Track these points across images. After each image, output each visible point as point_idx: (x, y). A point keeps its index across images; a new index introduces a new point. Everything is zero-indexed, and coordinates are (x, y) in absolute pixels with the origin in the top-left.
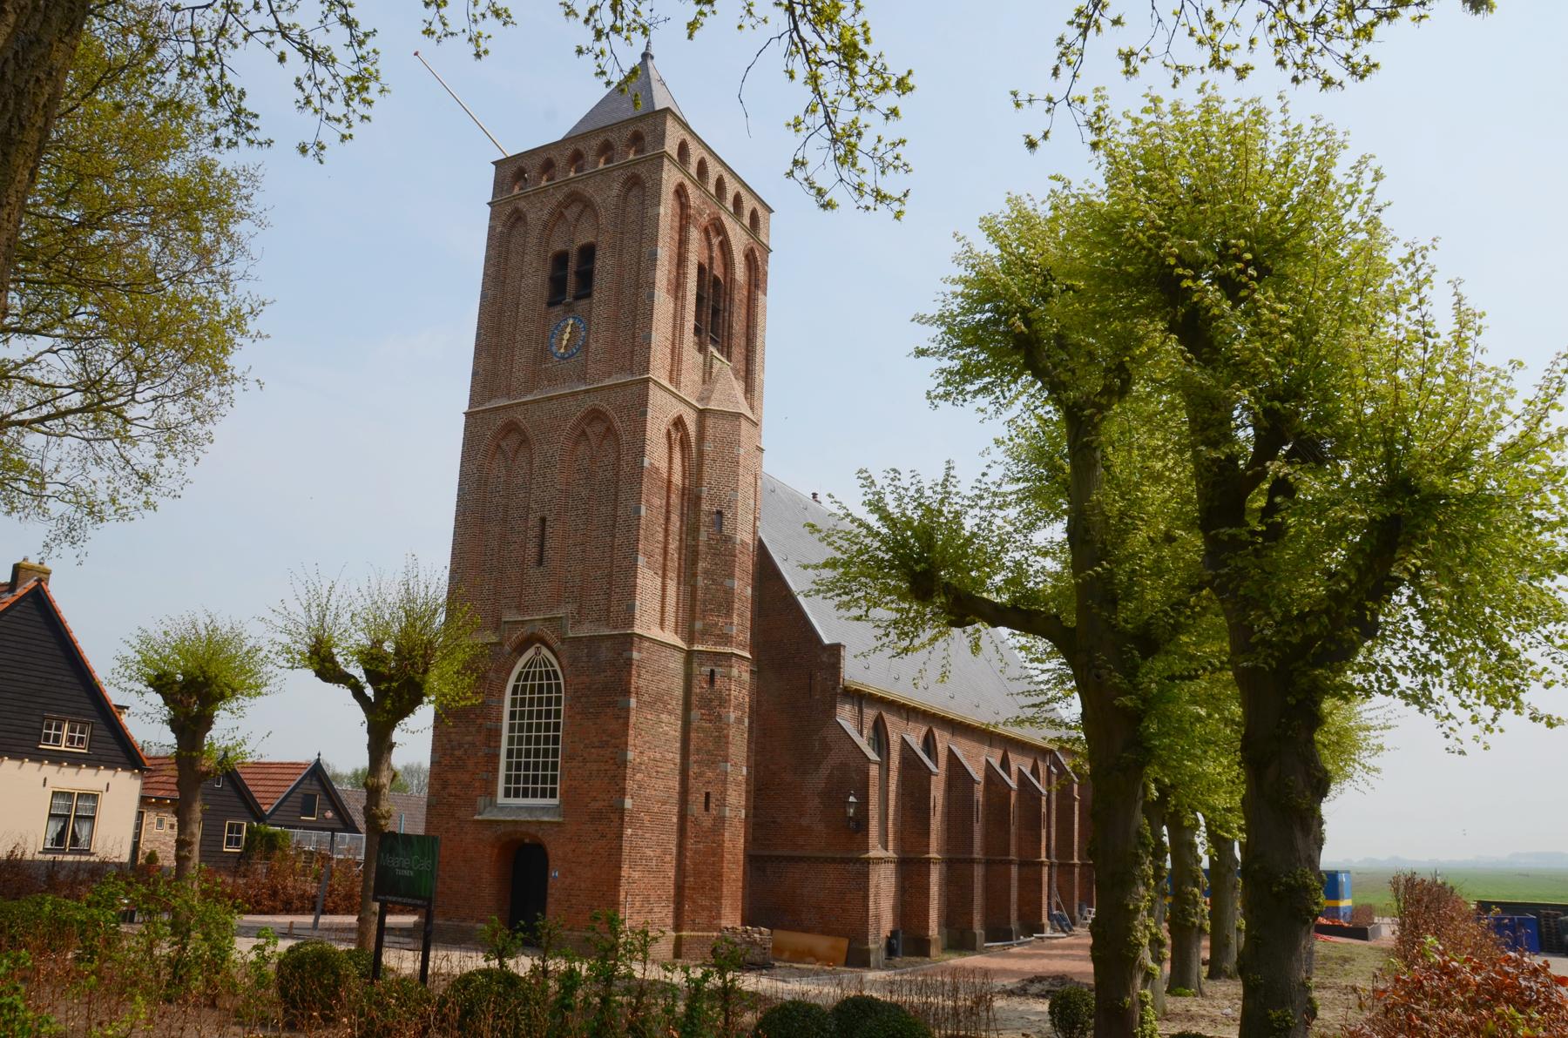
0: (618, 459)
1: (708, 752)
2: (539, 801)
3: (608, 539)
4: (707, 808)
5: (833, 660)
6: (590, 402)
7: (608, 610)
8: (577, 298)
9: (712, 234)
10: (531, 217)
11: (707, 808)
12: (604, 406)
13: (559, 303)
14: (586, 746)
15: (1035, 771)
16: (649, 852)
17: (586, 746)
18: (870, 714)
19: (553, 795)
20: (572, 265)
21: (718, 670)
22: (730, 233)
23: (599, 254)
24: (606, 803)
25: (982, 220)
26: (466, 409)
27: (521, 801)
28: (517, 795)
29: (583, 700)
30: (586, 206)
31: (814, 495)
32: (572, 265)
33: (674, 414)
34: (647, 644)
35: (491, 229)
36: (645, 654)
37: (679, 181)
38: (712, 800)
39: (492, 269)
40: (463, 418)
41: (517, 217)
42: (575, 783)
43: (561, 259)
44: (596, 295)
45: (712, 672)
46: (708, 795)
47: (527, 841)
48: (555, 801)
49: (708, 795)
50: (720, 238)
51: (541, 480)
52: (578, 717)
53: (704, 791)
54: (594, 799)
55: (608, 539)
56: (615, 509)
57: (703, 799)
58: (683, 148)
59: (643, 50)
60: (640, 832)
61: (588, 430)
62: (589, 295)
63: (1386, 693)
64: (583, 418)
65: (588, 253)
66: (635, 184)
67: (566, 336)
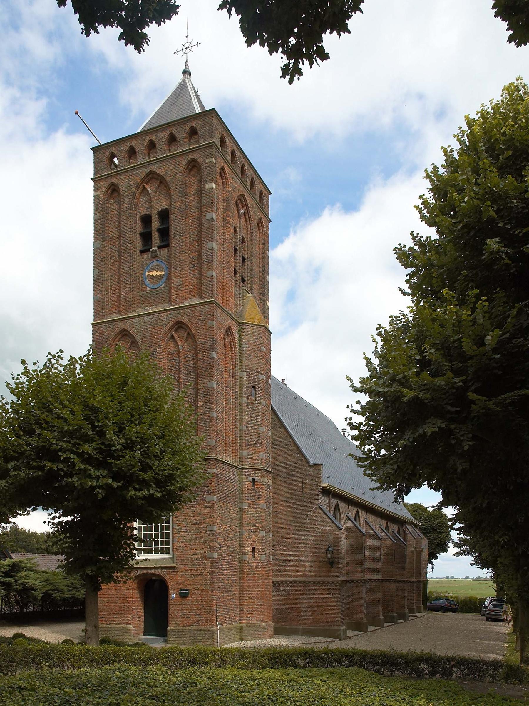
1: (253, 525)
4: (254, 556)
5: (316, 472)
6: (121, 326)
8: (160, 247)
9: (240, 206)
10: (123, 188)
11: (254, 556)
12: (128, 327)
13: (148, 250)
15: (399, 532)
18: (334, 501)
20: (156, 224)
23: (172, 217)
26: (92, 321)
30: (161, 182)
31: (283, 380)
32: (156, 224)
33: (226, 324)
35: (95, 197)
38: (257, 551)
39: (100, 226)
40: (91, 328)
41: (114, 189)
42: (182, 545)
43: (146, 220)
46: (254, 548)
47: (154, 578)
49: (254, 548)
53: (251, 547)
54: (195, 553)
57: (251, 551)
58: (223, 141)
59: (184, 68)
60: (221, 571)
61: (175, 334)
65: (164, 215)
66: (194, 166)
67: (155, 273)
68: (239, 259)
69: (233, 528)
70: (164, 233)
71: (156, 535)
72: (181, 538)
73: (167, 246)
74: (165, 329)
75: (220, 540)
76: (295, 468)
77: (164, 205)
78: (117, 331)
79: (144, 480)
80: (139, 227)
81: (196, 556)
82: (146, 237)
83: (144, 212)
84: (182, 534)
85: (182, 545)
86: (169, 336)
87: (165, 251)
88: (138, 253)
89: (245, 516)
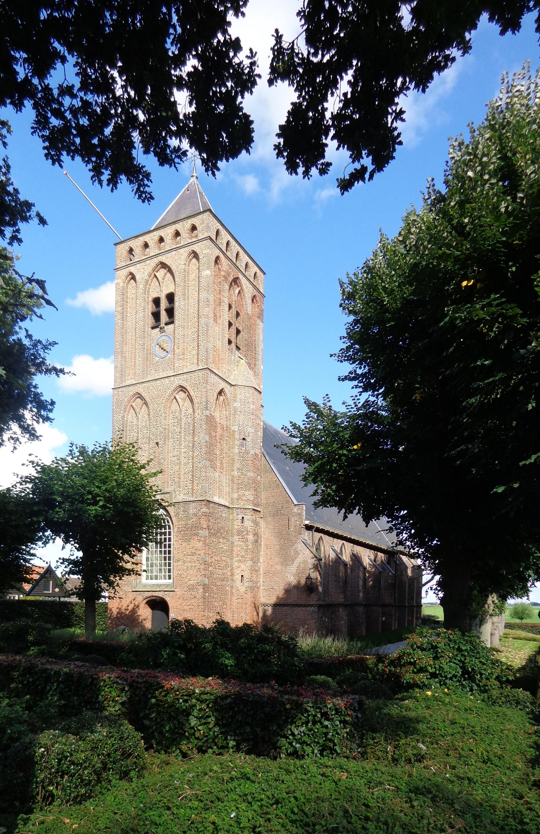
0: (194, 412)
2: (163, 581)
3: (191, 453)
7: (193, 489)
8: (167, 324)
12: (184, 384)
14: (185, 555)
16: (216, 604)
17: (185, 555)
19: (170, 578)
20: (164, 304)
21: (245, 517)
22: (244, 287)
24: (196, 582)
25: (298, 14)
27: (154, 582)
28: (152, 579)
29: (182, 533)
32: (164, 304)
34: (212, 505)
36: (211, 510)
37: (217, 255)
42: (180, 572)
43: (157, 301)
44: (176, 322)
45: (243, 518)
48: (171, 581)
50: (239, 288)
51: (155, 423)
52: (180, 541)
55: (191, 453)
56: (193, 438)
62: (172, 322)
63: (40, 342)
64: (174, 391)
65: (171, 297)
68: (233, 330)
69: (224, 558)
70: (170, 312)
71: (165, 539)
72: (179, 567)
73: (172, 322)
74: (169, 392)
75: (210, 569)
76: (282, 507)
77: (171, 290)
78: (131, 393)
79: (286, 694)
80: (150, 307)
81: (191, 582)
82: (156, 316)
83: (155, 295)
84: (180, 563)
85: (180, 572)
86: (172, 397)
87: (171, 326)
88: (150, 329)
89: (235, 548)
